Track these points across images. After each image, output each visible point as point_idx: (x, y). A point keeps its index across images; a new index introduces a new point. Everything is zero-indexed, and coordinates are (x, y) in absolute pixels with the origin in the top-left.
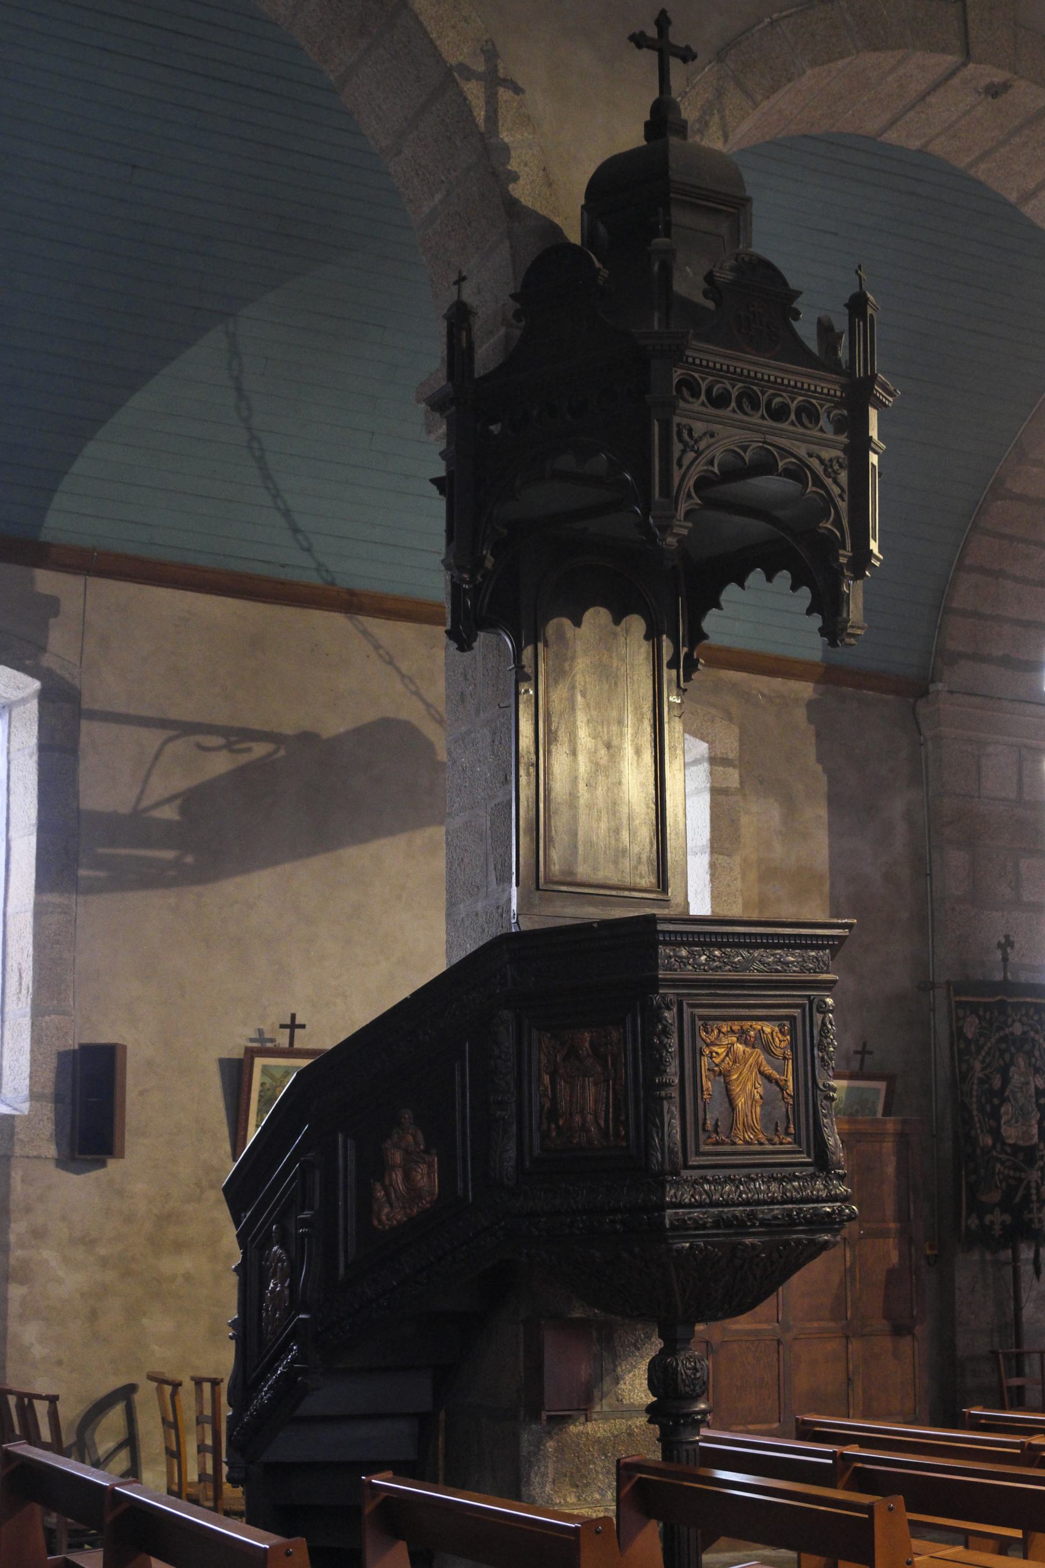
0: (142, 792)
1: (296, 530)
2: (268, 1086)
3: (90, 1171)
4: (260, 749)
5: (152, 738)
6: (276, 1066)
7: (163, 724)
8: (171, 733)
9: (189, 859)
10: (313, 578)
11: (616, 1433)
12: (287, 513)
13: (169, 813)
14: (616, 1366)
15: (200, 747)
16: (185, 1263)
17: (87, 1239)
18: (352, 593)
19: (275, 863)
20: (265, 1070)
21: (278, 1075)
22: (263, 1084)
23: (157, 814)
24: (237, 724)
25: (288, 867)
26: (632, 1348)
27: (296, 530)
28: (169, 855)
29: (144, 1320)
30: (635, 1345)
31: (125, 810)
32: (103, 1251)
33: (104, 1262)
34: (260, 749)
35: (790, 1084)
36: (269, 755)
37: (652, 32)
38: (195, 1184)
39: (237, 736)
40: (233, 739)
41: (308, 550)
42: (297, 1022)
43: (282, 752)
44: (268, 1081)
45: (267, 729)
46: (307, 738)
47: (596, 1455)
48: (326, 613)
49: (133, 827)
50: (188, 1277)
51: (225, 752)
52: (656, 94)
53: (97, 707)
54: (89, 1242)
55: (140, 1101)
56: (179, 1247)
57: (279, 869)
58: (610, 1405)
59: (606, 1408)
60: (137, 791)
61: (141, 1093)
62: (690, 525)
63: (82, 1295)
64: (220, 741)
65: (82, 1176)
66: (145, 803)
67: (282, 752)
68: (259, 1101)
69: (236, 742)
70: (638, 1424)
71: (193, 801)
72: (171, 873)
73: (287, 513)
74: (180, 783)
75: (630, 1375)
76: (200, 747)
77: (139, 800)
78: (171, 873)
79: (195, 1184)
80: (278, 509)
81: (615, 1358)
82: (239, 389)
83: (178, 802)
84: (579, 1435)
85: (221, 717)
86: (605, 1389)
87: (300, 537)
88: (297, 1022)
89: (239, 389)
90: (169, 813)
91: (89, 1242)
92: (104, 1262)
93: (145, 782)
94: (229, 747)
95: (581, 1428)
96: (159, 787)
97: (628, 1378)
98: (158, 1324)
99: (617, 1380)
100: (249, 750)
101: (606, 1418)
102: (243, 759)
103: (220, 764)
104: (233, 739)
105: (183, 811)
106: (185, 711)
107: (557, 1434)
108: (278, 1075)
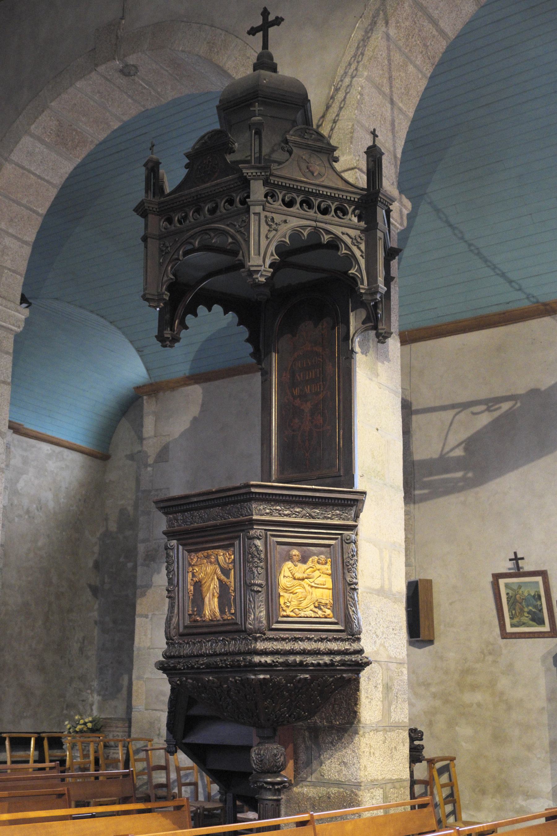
0: (444, 445)
1: (510, 282)
2: (510, 594)
3: (425, 647)
4: (505, 406)
5: (448, 415)
6: (513, 583)
7: (453, 406)
8: (456, 410)
9: (470, 475)
10: (526, 304)
11: (320, 795)
12: (503, 275)
13: (459, 452)
14: (320, 755)
15: (474, 414)
16: (478, 697)
17: (426, 683)
18: (545, 304)
19: (517, 468)
20: (507, 586)
21: (515, 587)
22: (507, 594)
23: (452, 454)
24: (492, 396)
25: (526, 468)
26: (330, 745)
27: (510, 282)
28: (459, 474)
29: (457, 728)
30: (332, 743)
31: (436, 456)
32: (433, 689)
33: (434, 696)
34: (505, 406)
35: (233, 584)
36: (510, 409)
37: (271, 18)
38: (481, 652)
39: (491, 403)
40: (490, 404)
41: (520, 289)
42: (513, 557)
43: (519, 404)
44: (510, 592)
45: (509, 394)
46: (534, 392)
47: (308, 808)
48: (539, 320)
49: (443, 464)
50: (479, 705)
51: (486, 413)
52: (259, 50)
53: (420, 407)
54: (427, 685)
55: (444, 608)
56: (474, 688)
57: (521, 470)
58: (317, 778)
59: (314, 780)
60: (441, 445)
61: (451, 604)
62: (272, 270)
63: (424, 712)
64: (483, 407)
65: (422, 650)
66: (447, 449)
67: (519, 404)
68: (508, 603)
69: (492, 406)
70: (334, 792)
71: (470, 444)
72: (461, 484)
73: (503, 275)
74: (464, 435)
75: (329, 761)
76: (474, 414)
77: (442, 451)
78: (461, 484)
79: (481, 652)
80: (498, 274)
81: (320, 750)
82: (450, 226)
83: (463, 445)
84: (298, 793)
85: (483, 394)
86: (314, 768)
87: (513, 284)
88: (513, 557)
89: (450, 226)
90: (459, 452)
91: (427, 685)
92: (434, 696)
93: (446, 439)
94: (488, 410)
95: (300, 790)
96: (452, 441)
97: (328, 762)
98: (465, 730)
99: (321, 763)
100: (500, 408)
101: (314, 785)
102: (496, 414)
103: (485, 419)
104: (490, 404)
105: (466, 449)
106: (464, 397)
107: (287, 792)
108: (515, 587)
